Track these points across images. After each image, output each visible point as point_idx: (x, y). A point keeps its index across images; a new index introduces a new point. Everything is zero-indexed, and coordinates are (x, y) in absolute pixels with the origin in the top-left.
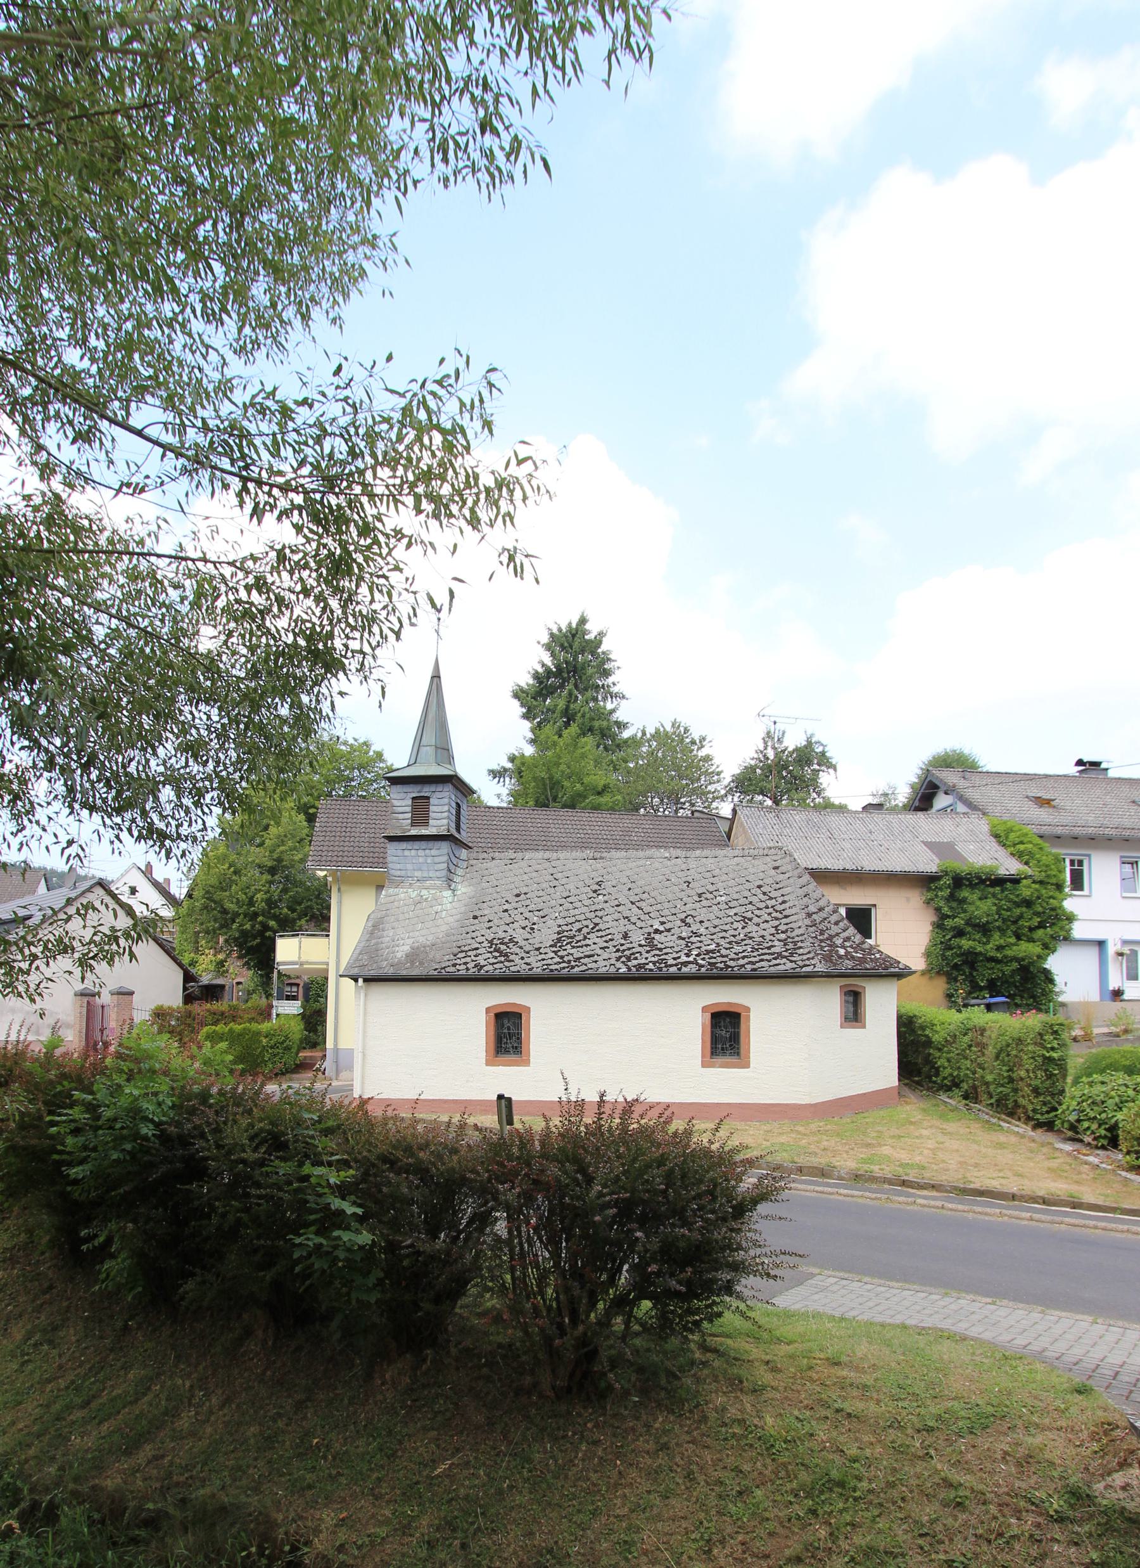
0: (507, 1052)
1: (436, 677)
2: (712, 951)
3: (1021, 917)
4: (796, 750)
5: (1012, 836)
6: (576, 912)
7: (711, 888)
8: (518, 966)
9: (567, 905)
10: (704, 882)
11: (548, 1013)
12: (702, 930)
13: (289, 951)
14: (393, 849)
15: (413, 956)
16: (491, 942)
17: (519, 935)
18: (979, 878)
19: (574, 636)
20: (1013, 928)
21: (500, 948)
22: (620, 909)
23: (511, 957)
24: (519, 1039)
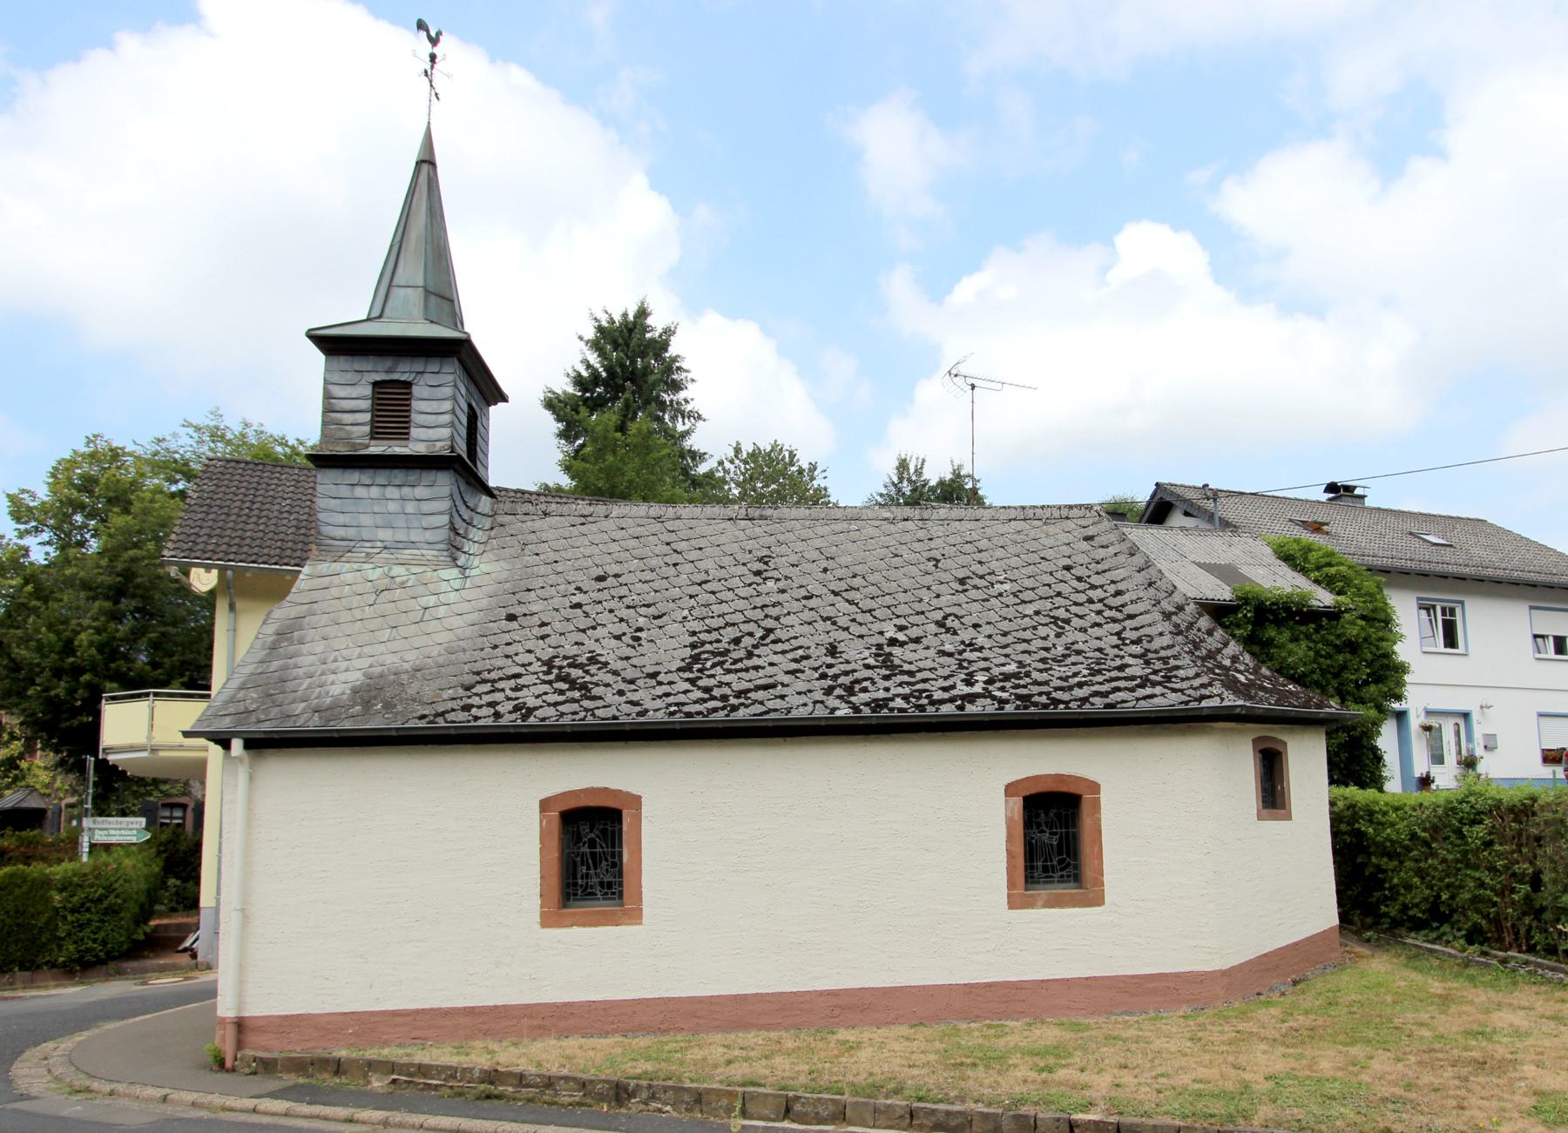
0: (589, 894)
1: (427, 161)
2: (1016, 676)
3: (1344, 667)
4: (941, 483)
5: (1313, 557)
6: (725, 608)
7: (981, 570)
8: (612, 707)
9: (704, 598)
10: (963, 560)
11: (681, 806)
12: (981, 641)
13: (131, 727)
14: (329, 483)
15: (367, 694)
16: (549, 664)
17: (610, 651)
18: (1287, 609)
19: (630, 331)
20: (1335, 683)
21: (567, 675)
22: (812, 603)
23: (596, 691)
24: (616, 865)
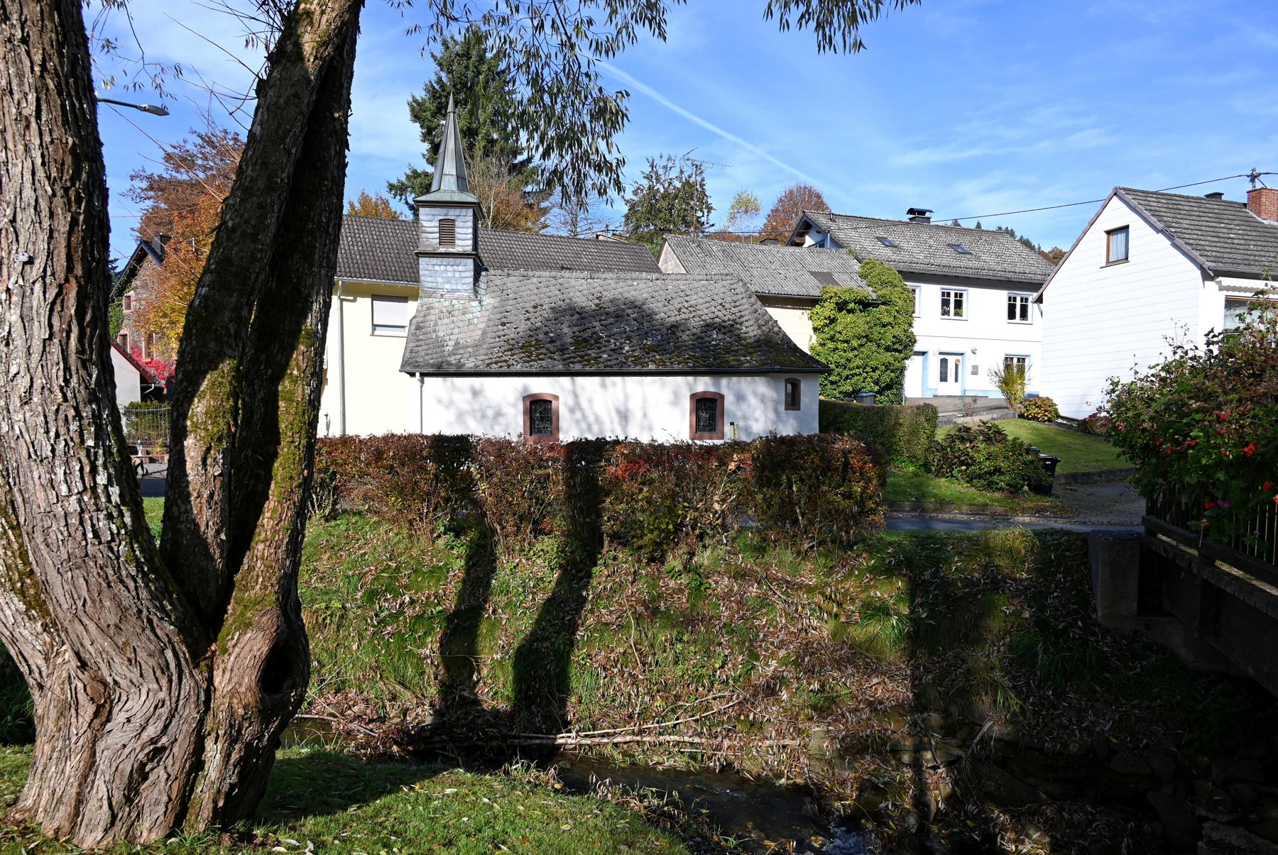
10: (679, 300)
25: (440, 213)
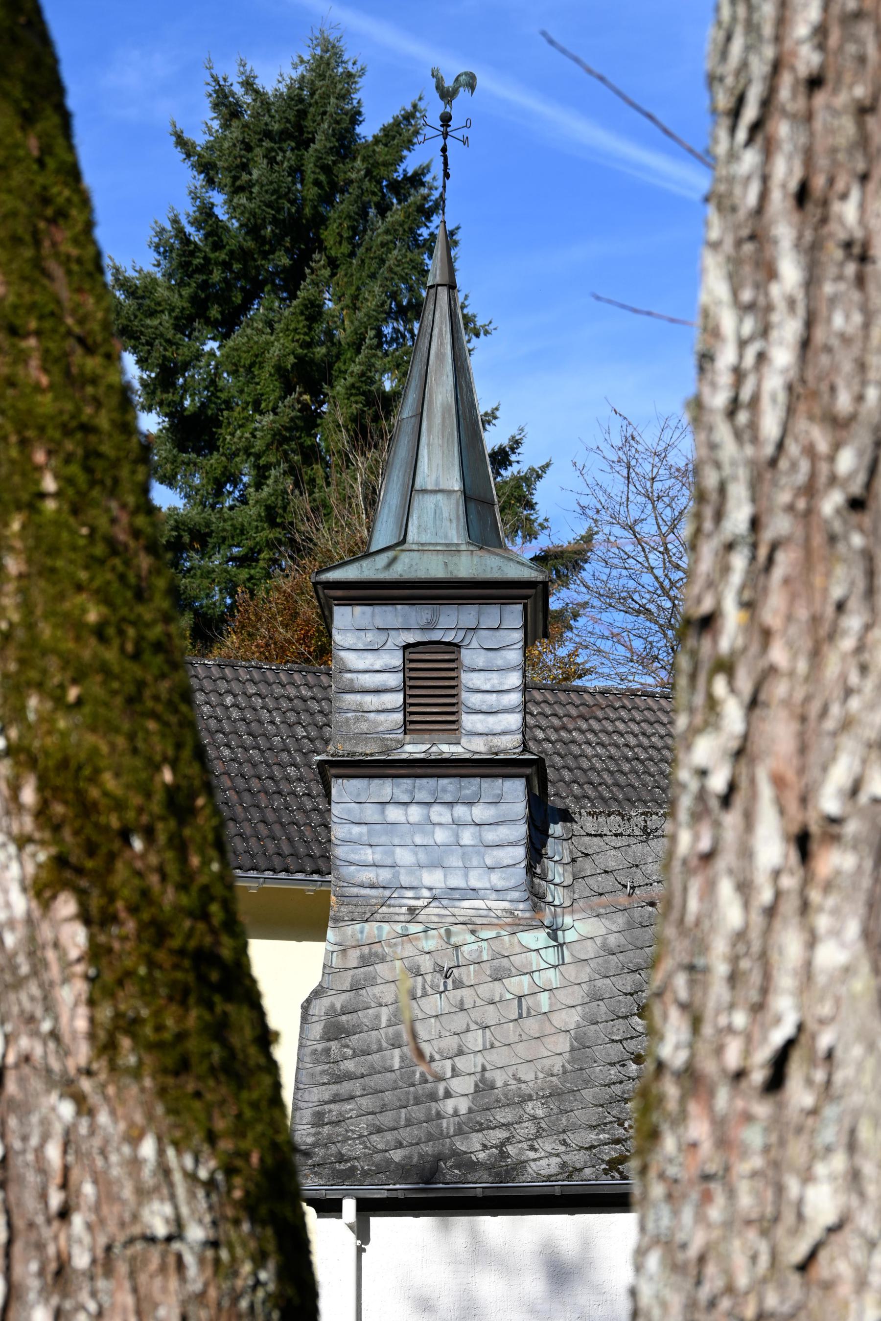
25: (407, 623)
